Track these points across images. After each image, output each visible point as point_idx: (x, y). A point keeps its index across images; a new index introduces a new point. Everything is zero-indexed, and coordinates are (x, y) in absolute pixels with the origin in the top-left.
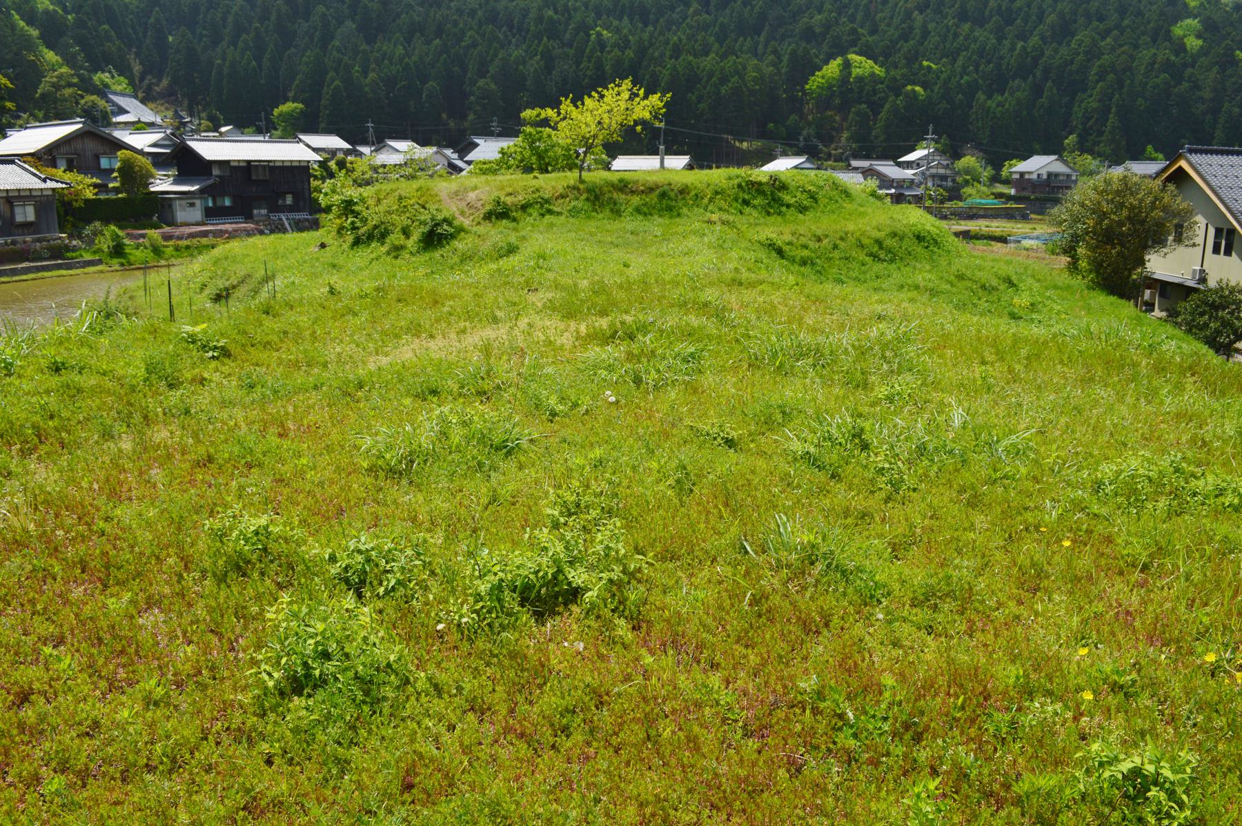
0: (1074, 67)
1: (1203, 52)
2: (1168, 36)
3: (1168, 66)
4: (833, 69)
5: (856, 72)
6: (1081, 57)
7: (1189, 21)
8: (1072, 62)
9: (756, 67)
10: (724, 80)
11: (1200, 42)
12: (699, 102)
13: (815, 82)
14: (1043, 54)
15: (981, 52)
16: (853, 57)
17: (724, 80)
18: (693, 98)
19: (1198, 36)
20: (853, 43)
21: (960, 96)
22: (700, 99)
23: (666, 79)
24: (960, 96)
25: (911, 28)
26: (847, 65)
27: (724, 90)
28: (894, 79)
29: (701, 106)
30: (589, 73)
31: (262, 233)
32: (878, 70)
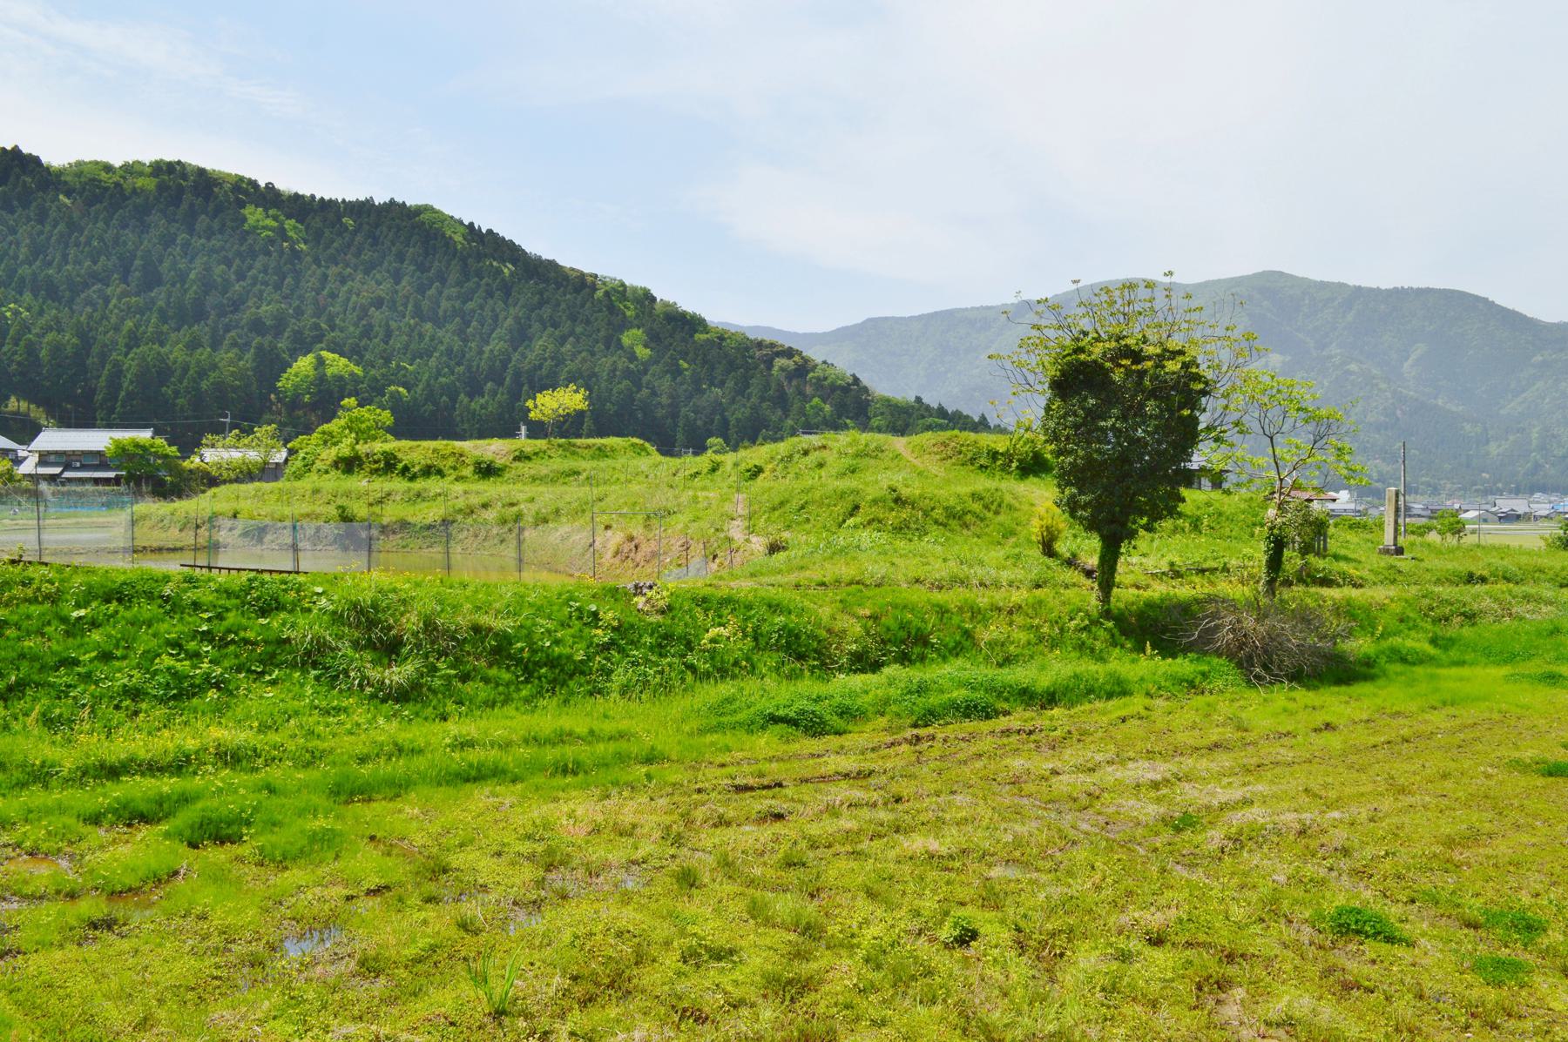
0: (544, 372)
1: (653, 361)
2: (620, 346)
3: (628, 374)
4: (304, 365)
5: (329, 372)
6: (549, 362)
7: (635, 331)
8: (540, 367)
9: (231, 363)
10: (202, 374)
11: (648, 351)
12: (176, 397)
13: (286, 382)
14: (510, 360)
15: (449, 352)
16: (324, 353)
17: (202, 374)
18: (167, 391)
19: (646, 346)
20: (319, 338)
21: (444, 398)
22: (177, 393)
23: (134, 370)
24: (444, 398)
25: (371, 326)
26: (321, 362)
27: (204, 385)
28: (375, 379)
29: (180, 401)
30: (17, 358)
31: (1197, 601)
32: (358, 371)
